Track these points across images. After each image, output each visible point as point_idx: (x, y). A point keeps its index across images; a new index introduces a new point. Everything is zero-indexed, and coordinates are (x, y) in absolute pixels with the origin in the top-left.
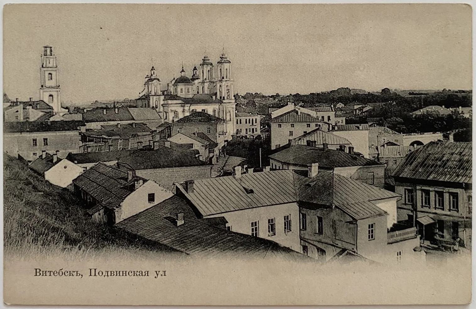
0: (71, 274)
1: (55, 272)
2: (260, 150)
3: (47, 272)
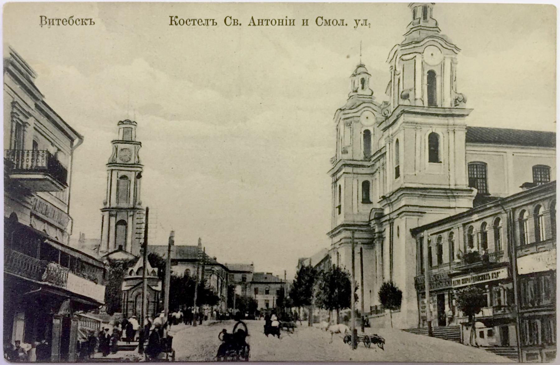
0: (84, 23)
1: (65, 20)
3: (54, 21)
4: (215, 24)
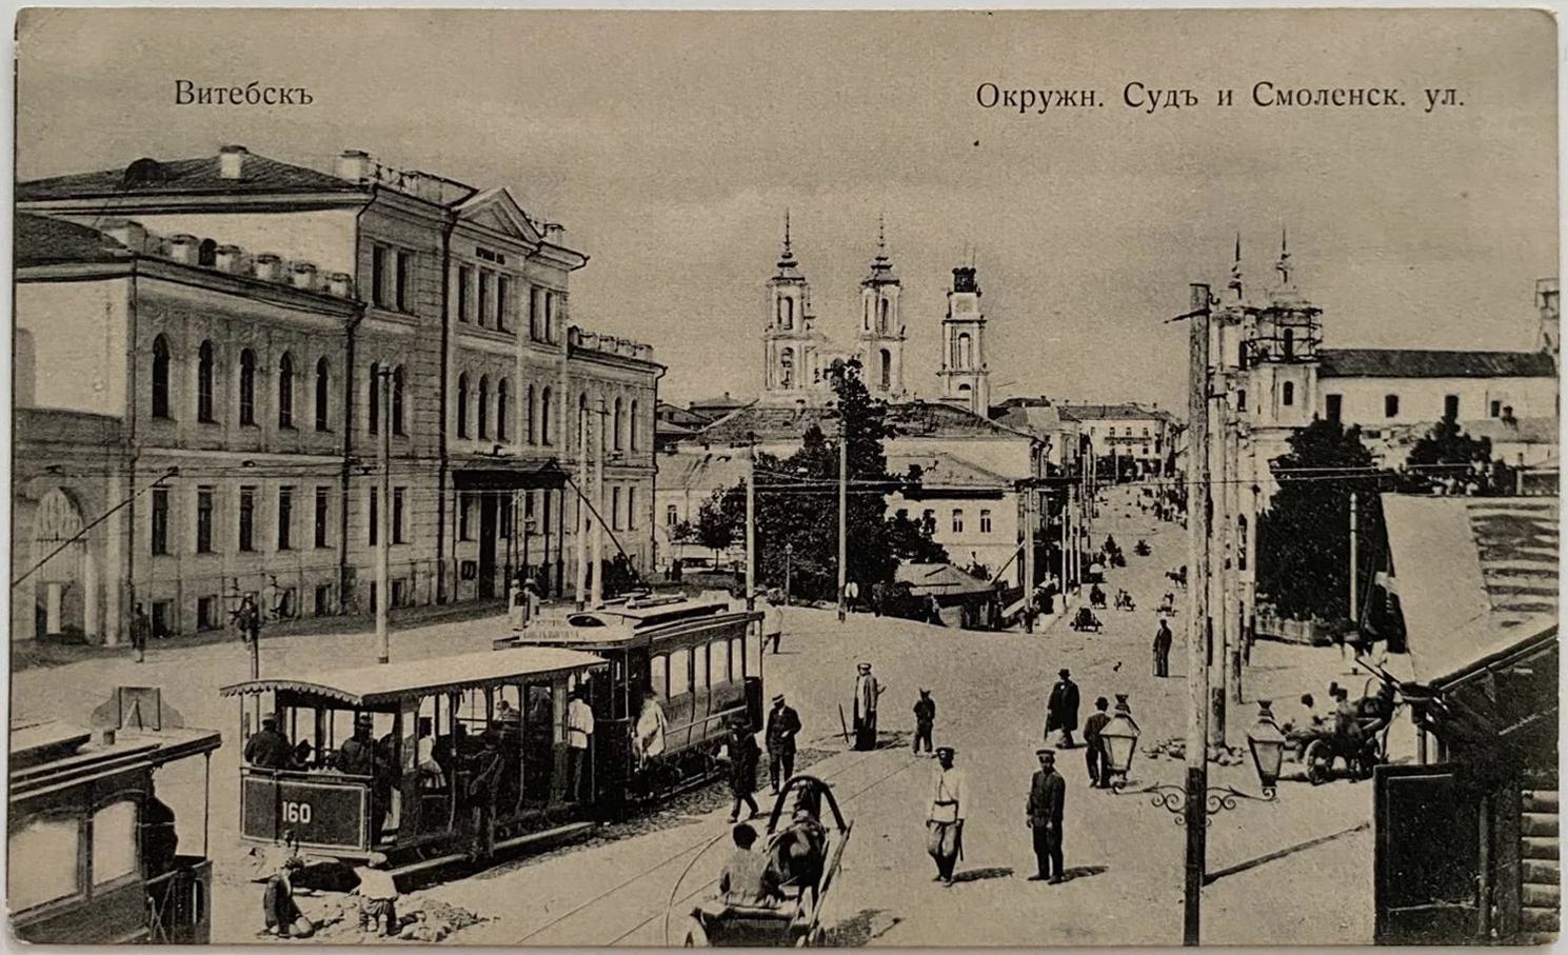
1: (236, 92)
2: (1505, 732)
3: (212, 92)
4: (1192, 101)
